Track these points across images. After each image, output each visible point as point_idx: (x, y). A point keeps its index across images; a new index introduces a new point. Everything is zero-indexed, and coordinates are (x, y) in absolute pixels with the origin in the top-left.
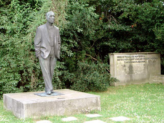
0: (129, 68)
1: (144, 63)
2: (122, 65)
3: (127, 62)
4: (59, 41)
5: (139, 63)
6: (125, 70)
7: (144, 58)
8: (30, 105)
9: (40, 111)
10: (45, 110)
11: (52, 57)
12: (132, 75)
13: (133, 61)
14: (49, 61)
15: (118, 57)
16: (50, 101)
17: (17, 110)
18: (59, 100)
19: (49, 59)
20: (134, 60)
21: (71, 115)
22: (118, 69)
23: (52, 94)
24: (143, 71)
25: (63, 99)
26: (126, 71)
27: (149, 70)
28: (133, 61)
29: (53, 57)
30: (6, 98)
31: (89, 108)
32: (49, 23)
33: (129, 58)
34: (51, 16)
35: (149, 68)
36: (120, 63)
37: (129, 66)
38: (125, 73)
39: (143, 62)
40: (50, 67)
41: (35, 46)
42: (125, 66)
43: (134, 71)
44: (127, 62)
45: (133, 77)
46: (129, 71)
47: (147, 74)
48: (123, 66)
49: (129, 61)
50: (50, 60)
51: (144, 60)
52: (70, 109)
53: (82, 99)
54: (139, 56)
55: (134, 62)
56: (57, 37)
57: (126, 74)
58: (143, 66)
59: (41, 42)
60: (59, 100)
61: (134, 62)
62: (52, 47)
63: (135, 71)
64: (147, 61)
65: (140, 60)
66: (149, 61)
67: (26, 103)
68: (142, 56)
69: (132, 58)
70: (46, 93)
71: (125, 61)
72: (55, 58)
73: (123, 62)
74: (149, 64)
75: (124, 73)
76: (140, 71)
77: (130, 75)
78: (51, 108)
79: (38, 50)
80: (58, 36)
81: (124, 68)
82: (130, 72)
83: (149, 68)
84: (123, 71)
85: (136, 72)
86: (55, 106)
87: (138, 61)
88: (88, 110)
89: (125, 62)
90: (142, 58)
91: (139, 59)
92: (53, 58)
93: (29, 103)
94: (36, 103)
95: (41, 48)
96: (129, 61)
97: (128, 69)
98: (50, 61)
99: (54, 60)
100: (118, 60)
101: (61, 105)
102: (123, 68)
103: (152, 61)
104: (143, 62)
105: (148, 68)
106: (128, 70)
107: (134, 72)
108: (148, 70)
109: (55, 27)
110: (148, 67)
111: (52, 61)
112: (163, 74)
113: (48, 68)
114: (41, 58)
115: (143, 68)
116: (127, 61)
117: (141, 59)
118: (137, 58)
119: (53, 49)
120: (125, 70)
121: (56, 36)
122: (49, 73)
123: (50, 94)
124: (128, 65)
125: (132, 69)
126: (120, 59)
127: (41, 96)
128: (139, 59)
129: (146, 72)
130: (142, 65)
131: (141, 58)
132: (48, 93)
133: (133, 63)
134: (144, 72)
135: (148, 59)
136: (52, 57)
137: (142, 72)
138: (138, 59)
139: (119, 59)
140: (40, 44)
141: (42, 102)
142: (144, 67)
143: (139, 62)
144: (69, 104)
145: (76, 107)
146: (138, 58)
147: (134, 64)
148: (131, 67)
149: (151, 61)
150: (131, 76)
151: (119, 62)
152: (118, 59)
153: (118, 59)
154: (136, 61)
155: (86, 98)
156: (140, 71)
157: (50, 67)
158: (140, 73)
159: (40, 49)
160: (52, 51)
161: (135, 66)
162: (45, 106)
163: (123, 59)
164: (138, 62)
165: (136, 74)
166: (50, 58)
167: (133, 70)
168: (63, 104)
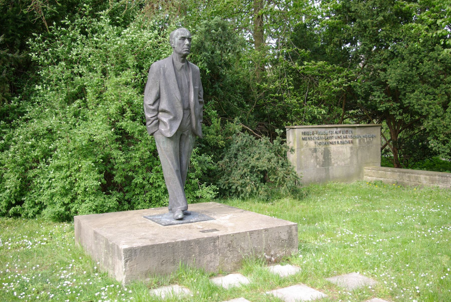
0: (324, 155)
1: (351, 145)
2: (310, 149)
3: (320, 144)
4: (199, 98)
5: (342, 145)
6: (317, 158)
7: (351, 135)
8: (138, 251)
9: (162, 264)
10: (174, 260)
11: (186, 133)
12: (328, 169)
13: (330, 141)
14: (178, 143)
15: (304, 133)
16: (184, 240)
17: (105, 258)
18: (206, 237)
19: (178, 138)
20: (334, 140)
21: (234, 270)
22: (302, 157)
23: (188, 219)
24: (349, 160)
25: (215, 234)
26: (318, 160)
27: (359, 158)
28: (330, 141)
29: (186, 135)
30: (79, 225)
31: (272, 253)
32: (177, 55)
33: (323, 136)
34: (182, 37)
35: (360, 154)
36: (307, 145)
37: (324, 151)
38: (316, 164)
39: (350, 143)
40: (180, 156)
41: (145, 109)
42: (315, 150)
43: (332, 160)
44: (320, 144)
45: (331, 171)
46: (323, 160)
47: (355, 166)
48: (313, 150)
49: (324, 141)
50: (181, 140)
51: (351, 140)
52: (231, 257)
53: (258, 231)
54: (342, 132)
55: (332, 143)
56: (197, 87)
57: (318, 166)
58: (349, 150)
59: (158, 99)
60: (205, 235)
61: (332, 143)
62: (185, 111)
63: (334, 159)
64: (357, 141)
65: (344, 140)
66: (360, 141)
67: (126, 247)
68: (347, 131)
69: (328, 136)
70: (171, 215)
71: (317, 141)
72: (190, 136)
73: (312, 143)
74: (360, 147)
75: (314, 164)
76: (343, 160)
77: (325, 168)
78: (188, 256)
79: (153, 118)
80: (199, 86)
81: (314, 154)
82: (325, 162)
83: (360, 154)
84: (312, 161)
85: (337, 163)
86: (197, 250)
87: (339, 140)
88: (272, 256)
89: (316, 143)
90: (348, 134)
91: (342, 137)
92: (187, 136)
93: (135, 245)
94: (153, 246)
95: (160, 113)
96: (324, 141)
97: (322, 156)
98: (180, 144)
99: (190, 140)
100: (303, 139)
101: (211, 248)
102: (313, 155)
103: (365, 141)
104: (349, 142)
105: (357, 155)
106: (321, 158)
107: (333, 162)
108: (357, 158)
109: (192, 65)
110: (357, 152)
111: (185, 143)
112: (447, 174)
113: (177, 160)
114: (161, 136)
115: (349, 155)
116: (321, 141)
117: (346, 137)
118: (339, 135)
119: (186, 116)
120: (317, 158)
121: (194, 85)
122: (179, 169)
123: (181, 219)
124: (321, 149)
125: (329, 157)
126: (307, 136)
127: (161, 224)
128: (342, 137)
129: (355, 162)
130: (348, 148)
131: (345, 135)
132: (177, 216)
133: (331, 146)
134: (351, 162)
135: (359, 137)
136: (184, 135)
137: (347, 162)
138: (341, 136)
139: (306, 137)
140: (156, 105)
141: (167, 241)
142: (351, 153)
143: (343, 143)
144: (229, 245)
145: (245, 251)
146: (341, 134)
147: (332, 148)
148: (327, 154)
149: (364, 142)
150: (327, 170)
151: (305, 142)
152: (304, 136)
153: (304, 136)
154: (336, 140)
155: (266, 230)
156: (343, 160)
157: (180, 156)
158: (343, 163)
159: (157, 115)
160: (185, 119)
161: (334, 151)
162: (174, 253)
163: (313, 136)
164: (339, 142)
165: (336, 165)
166: (181, 135)
167: (331, 159)
168: (215, 246)
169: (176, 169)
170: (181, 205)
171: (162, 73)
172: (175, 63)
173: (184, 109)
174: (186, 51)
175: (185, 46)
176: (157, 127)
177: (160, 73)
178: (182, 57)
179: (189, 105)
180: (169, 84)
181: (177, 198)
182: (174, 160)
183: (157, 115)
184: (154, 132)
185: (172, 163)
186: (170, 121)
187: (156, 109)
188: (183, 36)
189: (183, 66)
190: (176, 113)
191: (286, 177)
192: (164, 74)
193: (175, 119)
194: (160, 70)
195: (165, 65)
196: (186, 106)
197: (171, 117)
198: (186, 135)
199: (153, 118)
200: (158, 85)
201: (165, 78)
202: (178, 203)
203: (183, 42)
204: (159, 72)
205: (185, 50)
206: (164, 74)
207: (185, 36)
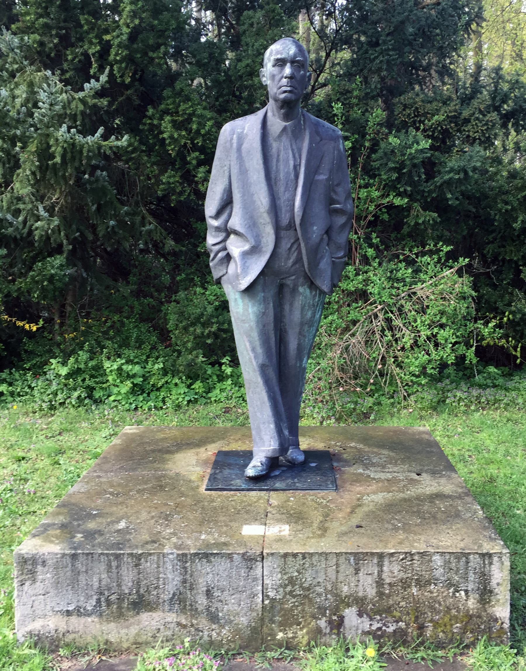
11: (289, 282)
92: (294, 290)
111: (291, 305)
119: (285, 245)
169: (260, 361)
170: (267, 443)
171: (235, 145)
172: (269, 123)
173: (278, 229)
174: (285, 92)
175: (284, 81)
176: (225, 265)
177: (231, 145)
178: (282, 107)
179: (293, 218)
180: (247, 171)
181: (261, 426)
182: (258, 344)
183: (224, 240)
184: (223, 276)
185: (253, 350)
186: (245, 254)
187: (223, 226)
188: (279, 56)
189: (285, 129)
190: (258, 238)
191: (472, 441)
192: (239, 149)
193: (255, 250)
194: (232, 139)
195: (244, 129)
196: (285, 221)
197: (247, 247)
198: (291, 286)
199: (217, 247)
200: (227, 174)
201: (240, 157)
202: (261, 439)
203: (281, 72)
204: (228, 144)
205: (284, 89)
206: (239, 149)
207: (283, 56)
